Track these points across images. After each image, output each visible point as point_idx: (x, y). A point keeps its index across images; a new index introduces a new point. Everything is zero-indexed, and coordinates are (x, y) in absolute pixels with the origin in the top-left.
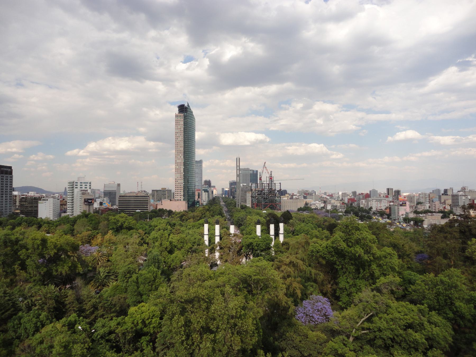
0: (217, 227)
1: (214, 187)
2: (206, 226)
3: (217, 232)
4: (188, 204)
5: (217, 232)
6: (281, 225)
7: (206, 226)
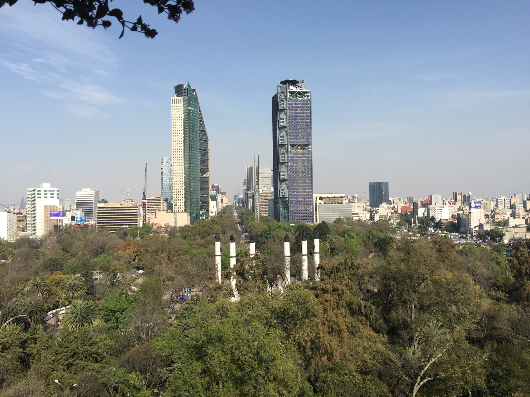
0: (233, 245)
1: (224, 193)
2: (218, 244)
3: (233, 253)
4: (191, 215)
5: (233, 253)
6: (317, 242)
7: (218, 244)
